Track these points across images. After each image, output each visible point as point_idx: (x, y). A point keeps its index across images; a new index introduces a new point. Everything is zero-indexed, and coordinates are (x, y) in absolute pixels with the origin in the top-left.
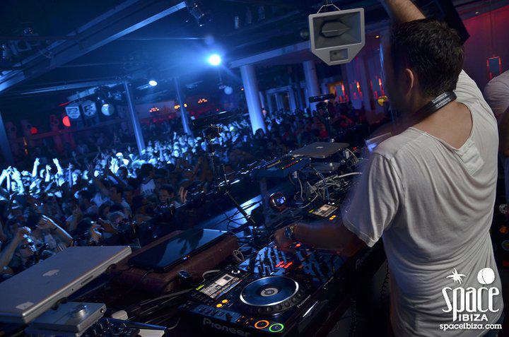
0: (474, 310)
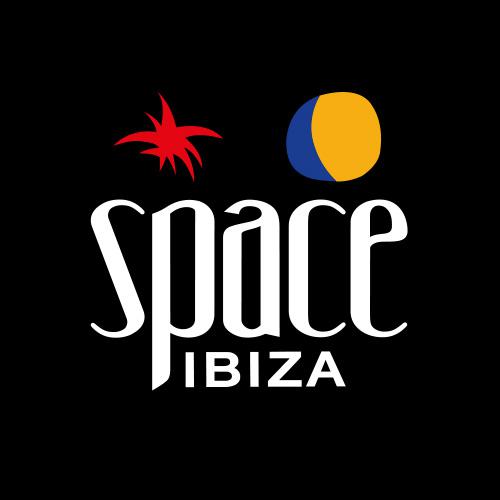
0: (270, 325)
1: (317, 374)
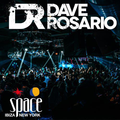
0: (28, 111)
1: (13, 116)
